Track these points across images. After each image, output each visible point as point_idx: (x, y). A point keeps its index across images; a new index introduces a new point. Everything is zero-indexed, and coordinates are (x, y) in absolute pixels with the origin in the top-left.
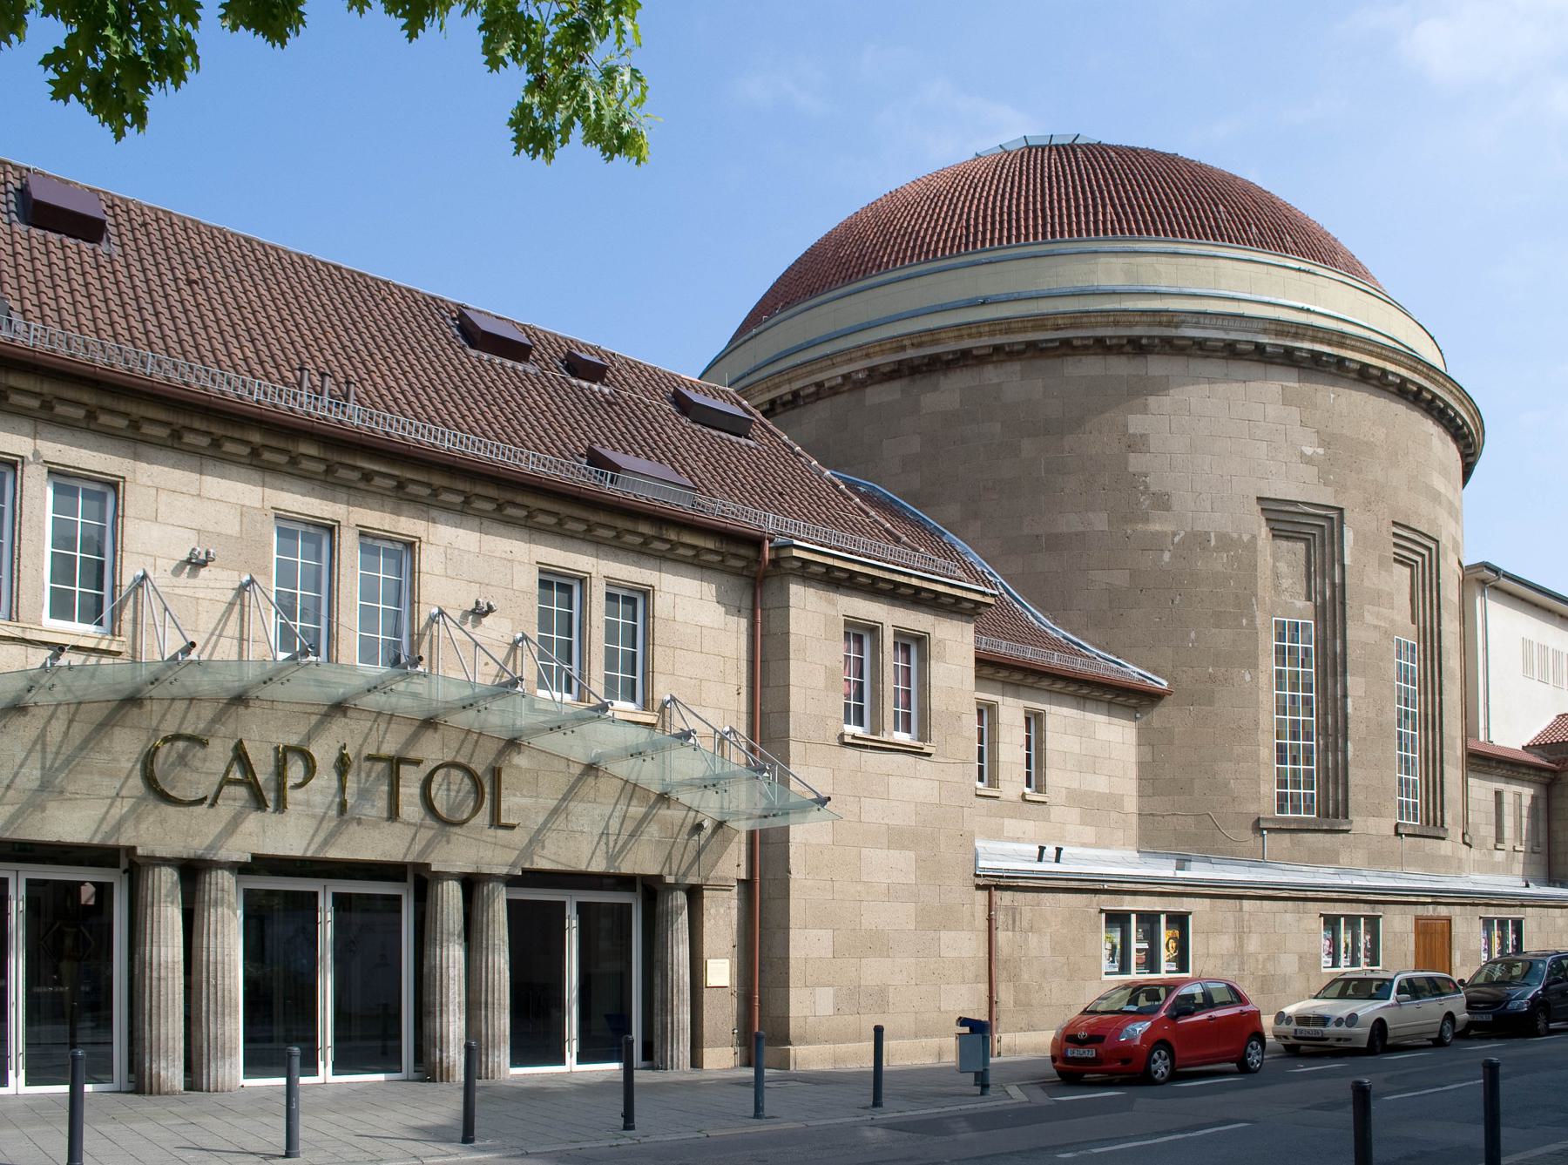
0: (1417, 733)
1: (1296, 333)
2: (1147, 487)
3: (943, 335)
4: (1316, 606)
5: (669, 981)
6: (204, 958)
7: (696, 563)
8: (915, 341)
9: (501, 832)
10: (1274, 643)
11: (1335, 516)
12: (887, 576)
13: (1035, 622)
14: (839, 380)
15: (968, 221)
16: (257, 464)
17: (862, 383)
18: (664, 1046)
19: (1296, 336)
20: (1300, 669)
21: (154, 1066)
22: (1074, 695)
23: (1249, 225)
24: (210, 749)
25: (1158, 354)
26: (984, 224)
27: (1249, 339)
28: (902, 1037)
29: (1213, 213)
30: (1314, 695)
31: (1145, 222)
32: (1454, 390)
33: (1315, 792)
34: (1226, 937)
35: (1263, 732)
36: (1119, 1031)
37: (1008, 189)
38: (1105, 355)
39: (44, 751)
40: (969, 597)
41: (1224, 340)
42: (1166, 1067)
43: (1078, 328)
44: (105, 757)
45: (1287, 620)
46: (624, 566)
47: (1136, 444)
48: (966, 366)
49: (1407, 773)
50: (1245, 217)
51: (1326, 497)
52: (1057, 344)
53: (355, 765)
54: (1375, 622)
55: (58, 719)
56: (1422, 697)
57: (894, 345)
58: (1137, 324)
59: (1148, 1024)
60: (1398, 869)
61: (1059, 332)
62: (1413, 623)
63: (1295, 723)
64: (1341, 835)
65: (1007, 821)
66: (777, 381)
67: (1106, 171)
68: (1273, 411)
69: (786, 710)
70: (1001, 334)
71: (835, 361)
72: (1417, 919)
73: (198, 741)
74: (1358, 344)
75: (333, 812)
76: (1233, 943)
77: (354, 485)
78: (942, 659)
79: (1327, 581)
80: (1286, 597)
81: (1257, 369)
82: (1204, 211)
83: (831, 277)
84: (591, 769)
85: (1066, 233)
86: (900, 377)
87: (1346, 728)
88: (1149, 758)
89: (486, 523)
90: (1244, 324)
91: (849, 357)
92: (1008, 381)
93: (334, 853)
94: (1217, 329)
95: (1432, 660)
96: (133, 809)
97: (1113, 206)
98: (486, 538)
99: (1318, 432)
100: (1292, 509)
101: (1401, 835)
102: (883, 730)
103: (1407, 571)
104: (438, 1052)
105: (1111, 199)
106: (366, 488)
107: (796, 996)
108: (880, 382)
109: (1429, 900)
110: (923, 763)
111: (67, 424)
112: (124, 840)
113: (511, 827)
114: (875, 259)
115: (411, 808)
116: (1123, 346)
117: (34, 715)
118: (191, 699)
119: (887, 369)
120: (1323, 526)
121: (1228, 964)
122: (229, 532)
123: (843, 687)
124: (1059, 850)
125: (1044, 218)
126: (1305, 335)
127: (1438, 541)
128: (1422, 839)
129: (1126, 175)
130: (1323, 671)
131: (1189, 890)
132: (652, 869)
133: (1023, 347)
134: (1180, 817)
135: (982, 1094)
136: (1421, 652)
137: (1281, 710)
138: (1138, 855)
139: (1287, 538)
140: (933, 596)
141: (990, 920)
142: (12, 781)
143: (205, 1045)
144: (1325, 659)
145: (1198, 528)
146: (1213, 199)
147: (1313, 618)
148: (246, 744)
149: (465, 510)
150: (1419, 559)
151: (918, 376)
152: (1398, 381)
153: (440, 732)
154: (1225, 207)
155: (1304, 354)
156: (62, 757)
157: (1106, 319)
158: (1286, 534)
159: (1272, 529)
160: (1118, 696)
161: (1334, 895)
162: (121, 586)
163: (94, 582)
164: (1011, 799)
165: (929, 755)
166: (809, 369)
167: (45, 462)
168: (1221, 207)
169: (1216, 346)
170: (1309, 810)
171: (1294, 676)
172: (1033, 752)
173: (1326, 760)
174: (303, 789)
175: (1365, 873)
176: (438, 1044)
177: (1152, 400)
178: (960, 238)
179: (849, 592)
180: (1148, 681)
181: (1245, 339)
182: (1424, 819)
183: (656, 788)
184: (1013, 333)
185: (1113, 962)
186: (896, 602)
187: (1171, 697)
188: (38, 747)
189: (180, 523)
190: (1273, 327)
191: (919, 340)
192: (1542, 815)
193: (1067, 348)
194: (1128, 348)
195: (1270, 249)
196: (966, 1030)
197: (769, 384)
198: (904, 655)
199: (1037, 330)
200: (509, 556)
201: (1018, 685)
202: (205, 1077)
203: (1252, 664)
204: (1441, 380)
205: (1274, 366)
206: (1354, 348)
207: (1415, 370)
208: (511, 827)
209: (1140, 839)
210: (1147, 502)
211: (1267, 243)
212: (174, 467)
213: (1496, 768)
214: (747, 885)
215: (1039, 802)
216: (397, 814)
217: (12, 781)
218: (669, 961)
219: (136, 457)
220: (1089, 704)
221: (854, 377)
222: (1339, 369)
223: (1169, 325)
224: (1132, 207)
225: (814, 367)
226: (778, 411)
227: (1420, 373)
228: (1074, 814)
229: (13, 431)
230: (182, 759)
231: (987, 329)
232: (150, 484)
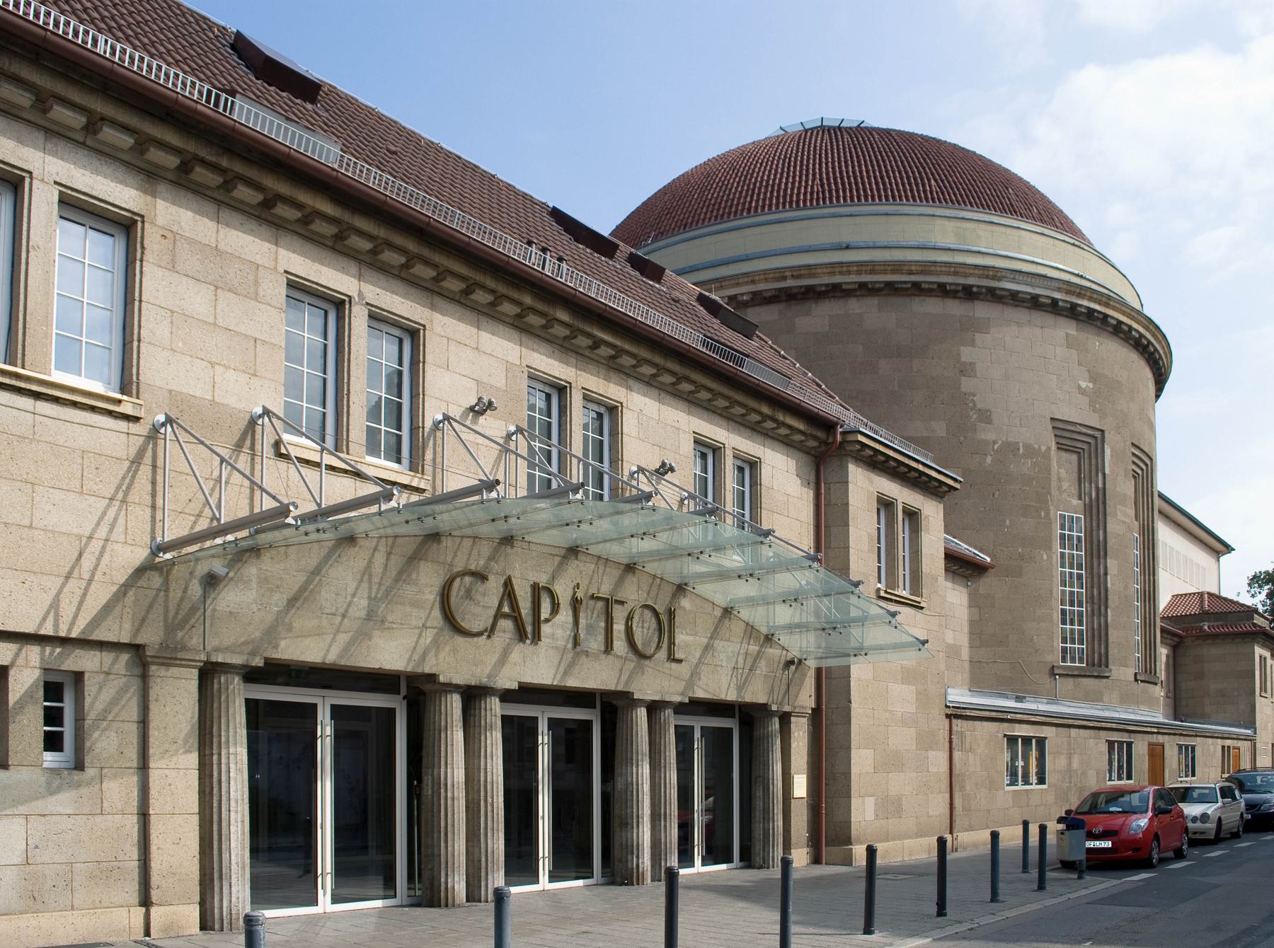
1: (1080, 293)
2: (975, 405)
3: (819, 271)
5: (771, 793)
6: (482, 779)
7: (786, 443)
8: (795, 273)
9: (674, 665)
11: (1099, 436)
15: (821, 180)
16: (520, 326)
18: (766, 849)
19: (1079, 295)
20: (1075, 552)
21: (449, 880)
24: (487, 584)
25: (982, 300)
26: (836, 184)
27: (1048, 295)
28: (910, 837)
30: (1083, 572)
33: (1084, 647)
38: (943, 297)
39: (370, 582)
41: (1030, 294)
44: (415, 589)
46: (743, 440)
47: (967, 370)
48: (834, 297)
52: (909, 286)
53: (584, 603)
54: (1123, 519)
55: (379, 551)
57: (777, 275)
58: (971, 275)
61: (912, 276)
63: (1072, 593)
64: (1104, 680)
68: (1061, 351)
71: (723, 284)
72: (1150, 744)
73: (481, 577)
74: (1117, 305)
75: (570, 646)
77: (581, 351)
79: (1093, 485)
81: (1049, 319)
84: (727, 612)
85: (883, 197)
86: (779, 302)
88: (977, 618)
89: (663, 395)
91: (736, 281)
92: (868, 311)
93: (573, 682)
94: (1027, 285)
96: (435, 641)
97: (936, 181)
98: (664, 408)
99: (1088, 370)
100: (1072, 428)
104: (635, 859)
105: (933, 174)
106: (589, 355)
107: (855, 803)
108: (760, 305)
111: (384, 270)
112: (427, 670)
113: (680, 661)
115: (620, 645)
117: (361, 547)
118: (475, 537)
119: (769, 294)
122: (498, 385)
125: (884, 184)
130: (1090, 554)
132: (762, 699)
133: (882, 286)
139: (1066, 450)
141: (951, 742)
142: (347, 611)
143: (483, 859)
145: (1011, 439)
148: (514, 581)
149: (651, 382)
151: (793, 302)
153: (636, 576)
156: (383, 588)
157: (948, 269)
159: (1057, 443)
160: (961, 567)
161: (1114, 726)
162: (423, 428)
163: (395, 423)
165: (922, 608)
167: (367, 304)
170: (1081, 661)
171: (1071, 557)
173: (1093, 622)
174: (550, 623)
175: (1118, 709)
176: (635, 851)
177: (979, 337)
181: (1045, 294)
183: (764, 630)
184: (876, 274)
188: (366, 577)
189: (464, 373)
190: (1065, 287)
191: (798, 273)
192: (1171, 670)
193: (917, 289)
200: (676, 425)
202: (483, 889)
203: (1049, 548)
206: (1114, 308)
208: (680, 661)
210: (975, 417)
212: (459, 320)
214: (816, 715)
216: (612, 649)
217: (347, 611)
218: (771, 776)
219: (433, 307)
221: (740, 298)
223: (994, 278)
229: (343, 270)
230: (468, 594)
231: (855, 268)
232: (443, 334)
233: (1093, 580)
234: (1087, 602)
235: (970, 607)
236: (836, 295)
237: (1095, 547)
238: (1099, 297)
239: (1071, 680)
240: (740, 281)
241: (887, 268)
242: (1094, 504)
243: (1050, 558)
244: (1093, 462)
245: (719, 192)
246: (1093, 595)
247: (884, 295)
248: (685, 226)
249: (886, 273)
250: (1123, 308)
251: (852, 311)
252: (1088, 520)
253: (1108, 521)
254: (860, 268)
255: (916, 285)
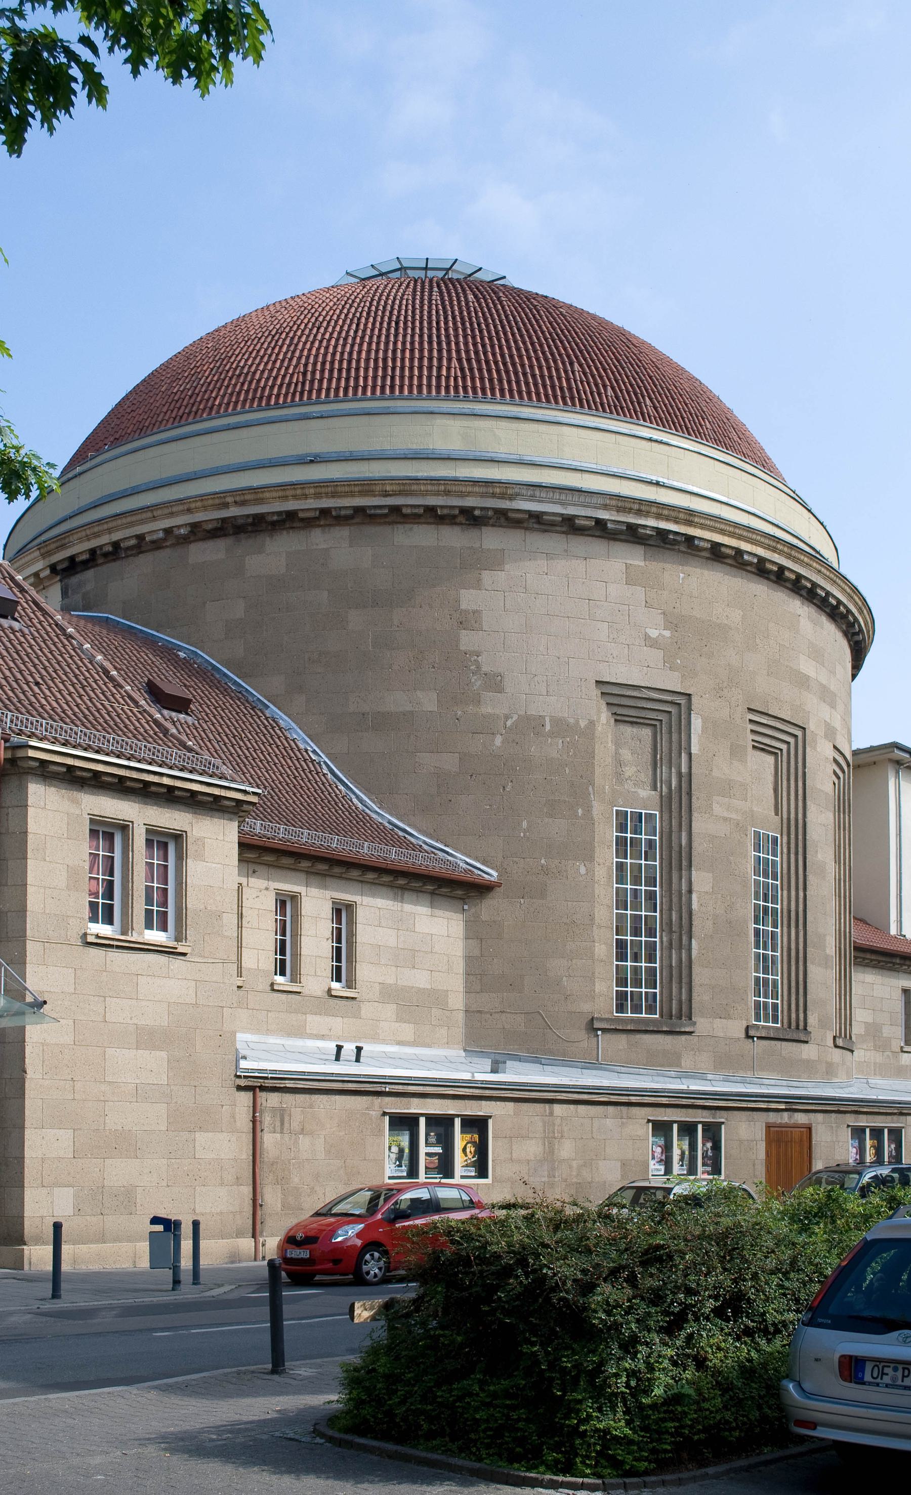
0: (779, 930)
2: (479, 667)
3: (267, 495)
4: (661, 796)
8: (238, 499)
10: (615, 834)
12: (135, 775)
13: (360, 805)
14: (161, 535)
15: (306, 365)
17: (184, 539)
19: (639, 513)
22: (390, 886)
23: (605, 386)
25: (493, 526)
29: (566, 372)
30: (657, 889)
31: (491, 380)
32: (823, 569)
33: (657, 991)
34: (533, 1142)
35: (600, 927)
36: (333, 1232)
37: (396, 307)
38: (437, 524)
40: (228, 795)
42: (380, 1269)
43: (407, 495)
45: (629, 810)
48: (292, 528)
49: (766, 971)
50: (601, 377)
51: (672, 681)
52: (386, 511)
54: (726, 814)
56: (785, 892)
57: (217, 501)
58: (469, 494)
59: (362, 1226)
60: (749, 1074)
62: (777, 814)
63: (636, 919)
64: (683, 1038)
65: (310, 1018)
66: (96, 529)
67: (458, 319)
68: (615, 590)
69: (22, 910)
70: (327, 497)
71: (155, 514)
72: (769, 1127)
76: (541, 1149)
78: (200, 857)
79: (673, 770)
80: (629, 786)
81: (598, 546)
82: (557, 370)
83: (162, 414)
86: (225, 535)
87: (691, 925)
88: (477, 952)
90: (582, 499)
91: (170, 510)
95: (797, 854)
97: (459, 360)
101: (752, 1037)
102: (133, 929)
103: (770, 759)
105: (458, 351)
108: (203, 539)
109: (783, 1107)
110: (176, 963)
114: (208, 400)
116: (454, 517)
119: (209, 526)
120: (670, 712)
121: (535, 1170)
123: (86, 886)
124: (359, 1049)
126: (648, 512)
127: (804, 729)
128: (778, 1043)
129: (479, 325)
130: (668, 866)
131: (488, 1093)
134: (509, 1015)
135: (173, 1289)
136: (785, 846)
137: (622, 904)
138: (463, 1054)
140: (189, 795)
144: (671, 852)
145: (532, 712)
146: (568, 356)
147: (658, 808)
150: (784, 747)
151: (242, 535)
152: (755, 561)
154: (581, 365)
155: (648, 532)
157: (436, 488)
158: (631, 719)
161: (664, 1101)
164: (315, 994)
165: (184, 954)
166: (129, 519)
168: (576, 366)
169: (554, 521)
170: (651, 1009)
172: (344, 945)
173: (670, 957)
175: (710, 1077)
177: (486, 576)
178: (296, 385)
179: (95, 791)
180: (476, 871)
182: (785, 1021)
184: (340, 497)
185: (682, 1165)
186: (148, 800)
187: (501, 890)
190: (614, 503)
191: (242, 498)
193: (397, 515)
194: (461, 519)
195: (625, 416)
196: (160, 1228)
197: (88, 532)
198: (161, 853)
199: (365, 496)
201: (325, 875)
203: (589, 857)
204: (806, 559)
205: (618, 543)
206: (703, 527)
207: (774, 550)
209: (466, 1037)
211: (622, 408)
213: (901, 965)
215: (347, 998)
220: (407, 895)
221: (176, 532)
222: (689, 547)
223: (502, 496)
224: (478, 361)
225: (134, 518)
226: (100, 561)
227: (780, 553)
228: (390, 1010)
231: (312, 491)
233: (671, 900)
234: (662, 930)
235: (467, 938)
236: (295, 525)
237: (674, 855)
238: (673, 514)
239: (623, 1037)
240: (175, 509)
241: (353, 488)
242: (675, 796)
243: (590, 872)
244: (675, 737)
245: (259, 364)
246: (671, 921)
247: (357, 524)
248: (179, 420)
249: (353, 496)
250: (718, 525)
251: (315, 547)
252: (666, 817)
253: (693, 818)
254: (318, 490)
255: (396, 510)
